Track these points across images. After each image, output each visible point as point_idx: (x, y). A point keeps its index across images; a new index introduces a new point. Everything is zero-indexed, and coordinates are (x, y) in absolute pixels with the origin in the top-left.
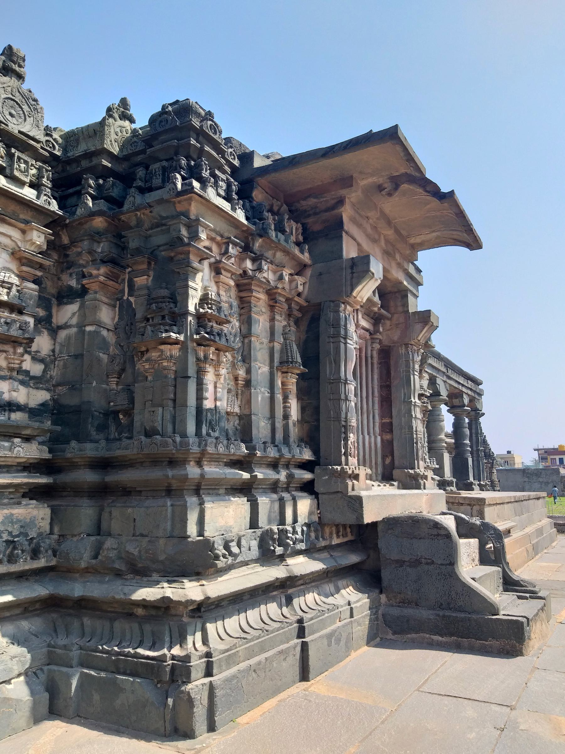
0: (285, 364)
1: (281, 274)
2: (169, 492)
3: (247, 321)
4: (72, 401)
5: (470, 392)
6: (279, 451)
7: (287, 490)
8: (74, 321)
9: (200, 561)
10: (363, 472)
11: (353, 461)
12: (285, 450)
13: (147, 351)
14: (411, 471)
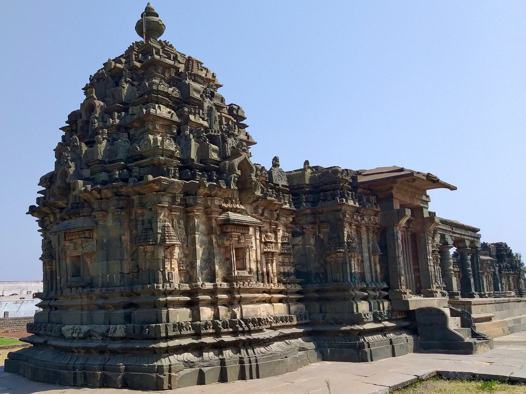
0: (374, 252)
1: (372, 218)
2: (345, 299)
3: (360, 239)
4: (304, 270)
5: (470, 238)
6: (376, 285)
7: (379, 299)
8: (300, 243)
9: (359, 319)
10: (408, 291)
11: (404, 287)
12: (378, 285)
13: (330, 254)
14: (430, 290)
